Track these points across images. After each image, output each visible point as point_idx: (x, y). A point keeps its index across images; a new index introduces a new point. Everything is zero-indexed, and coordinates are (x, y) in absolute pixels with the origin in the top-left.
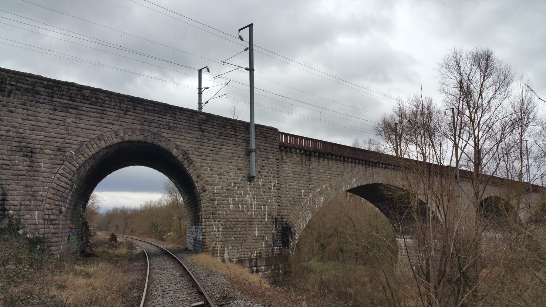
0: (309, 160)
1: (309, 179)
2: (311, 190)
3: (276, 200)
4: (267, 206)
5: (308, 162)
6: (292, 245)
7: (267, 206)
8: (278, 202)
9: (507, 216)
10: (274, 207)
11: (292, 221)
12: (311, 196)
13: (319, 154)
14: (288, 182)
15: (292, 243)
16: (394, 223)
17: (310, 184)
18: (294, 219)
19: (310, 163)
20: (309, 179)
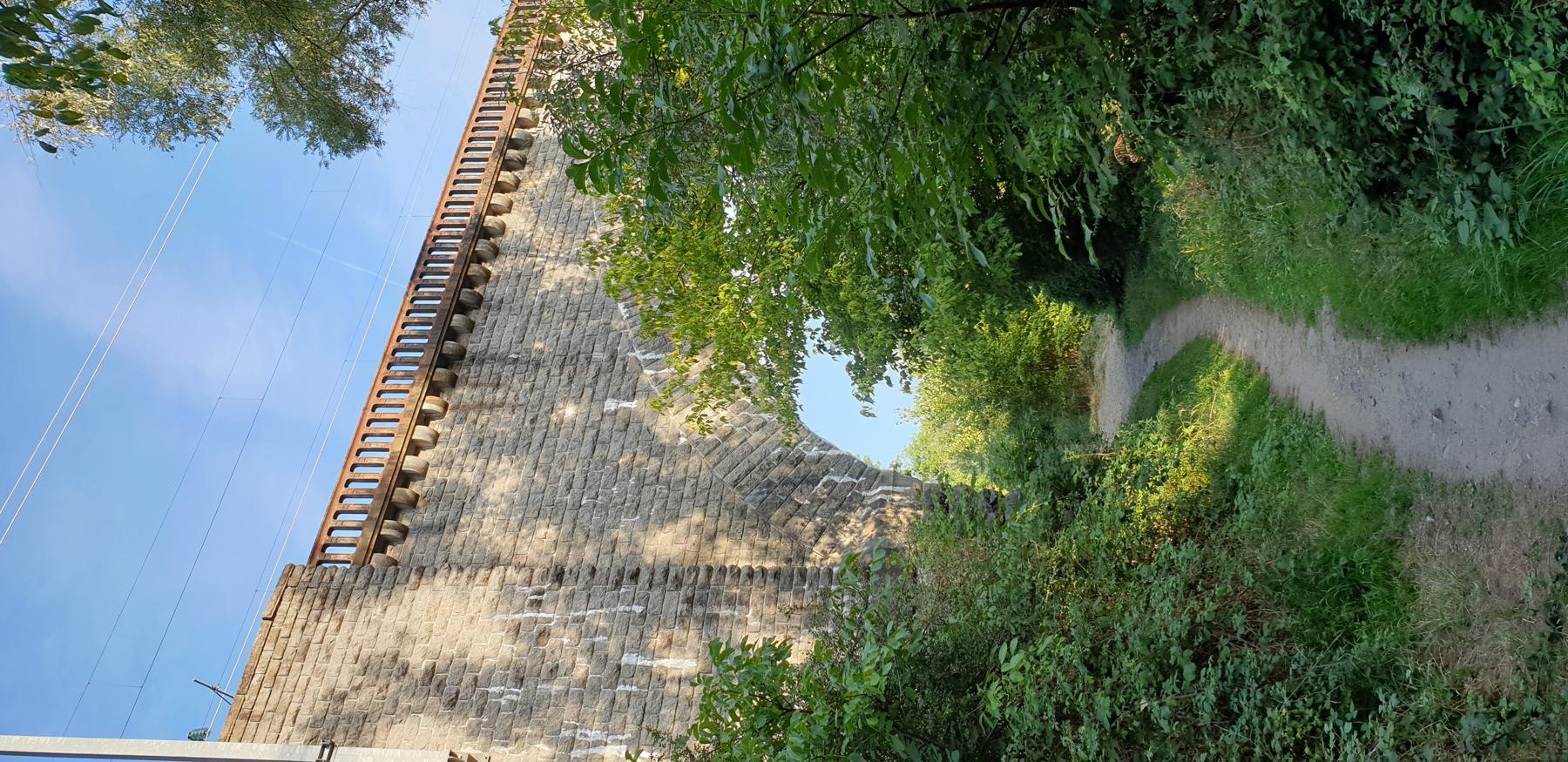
0: (482, 362)
1: (562, 367)
2: (613, 357)
3: (609, 595)
4: (624, 660)
5: (486, 369)
6: (847, 479)
7: (624, 660)
8: (618, 584)
9: (1287, 696)
10: (638, 609)
11: (734, 475)
12: (641, 358)
13: (462, 308)
14: (555, 491)
15: (836, 479)
16: (1321, 28)
17: (589, 360)
18: (727, 462)
19: (493, 358)
20: (562, 367)
